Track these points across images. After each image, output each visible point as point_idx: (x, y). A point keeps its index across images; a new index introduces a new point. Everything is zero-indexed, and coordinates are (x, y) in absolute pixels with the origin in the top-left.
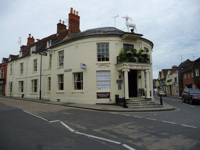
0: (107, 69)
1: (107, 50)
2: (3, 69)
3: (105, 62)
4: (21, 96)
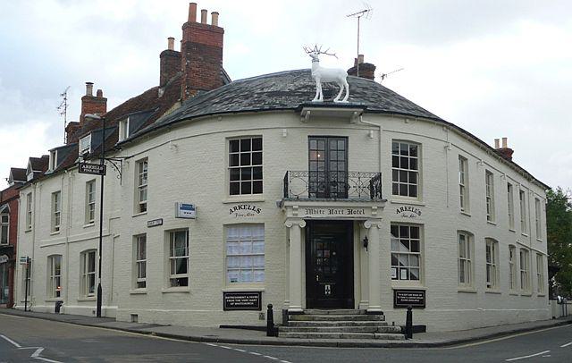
0: (256, 219)
1: (258, 159)
2: (6, 211)
3: (408, 199)
4: (53, 306)
